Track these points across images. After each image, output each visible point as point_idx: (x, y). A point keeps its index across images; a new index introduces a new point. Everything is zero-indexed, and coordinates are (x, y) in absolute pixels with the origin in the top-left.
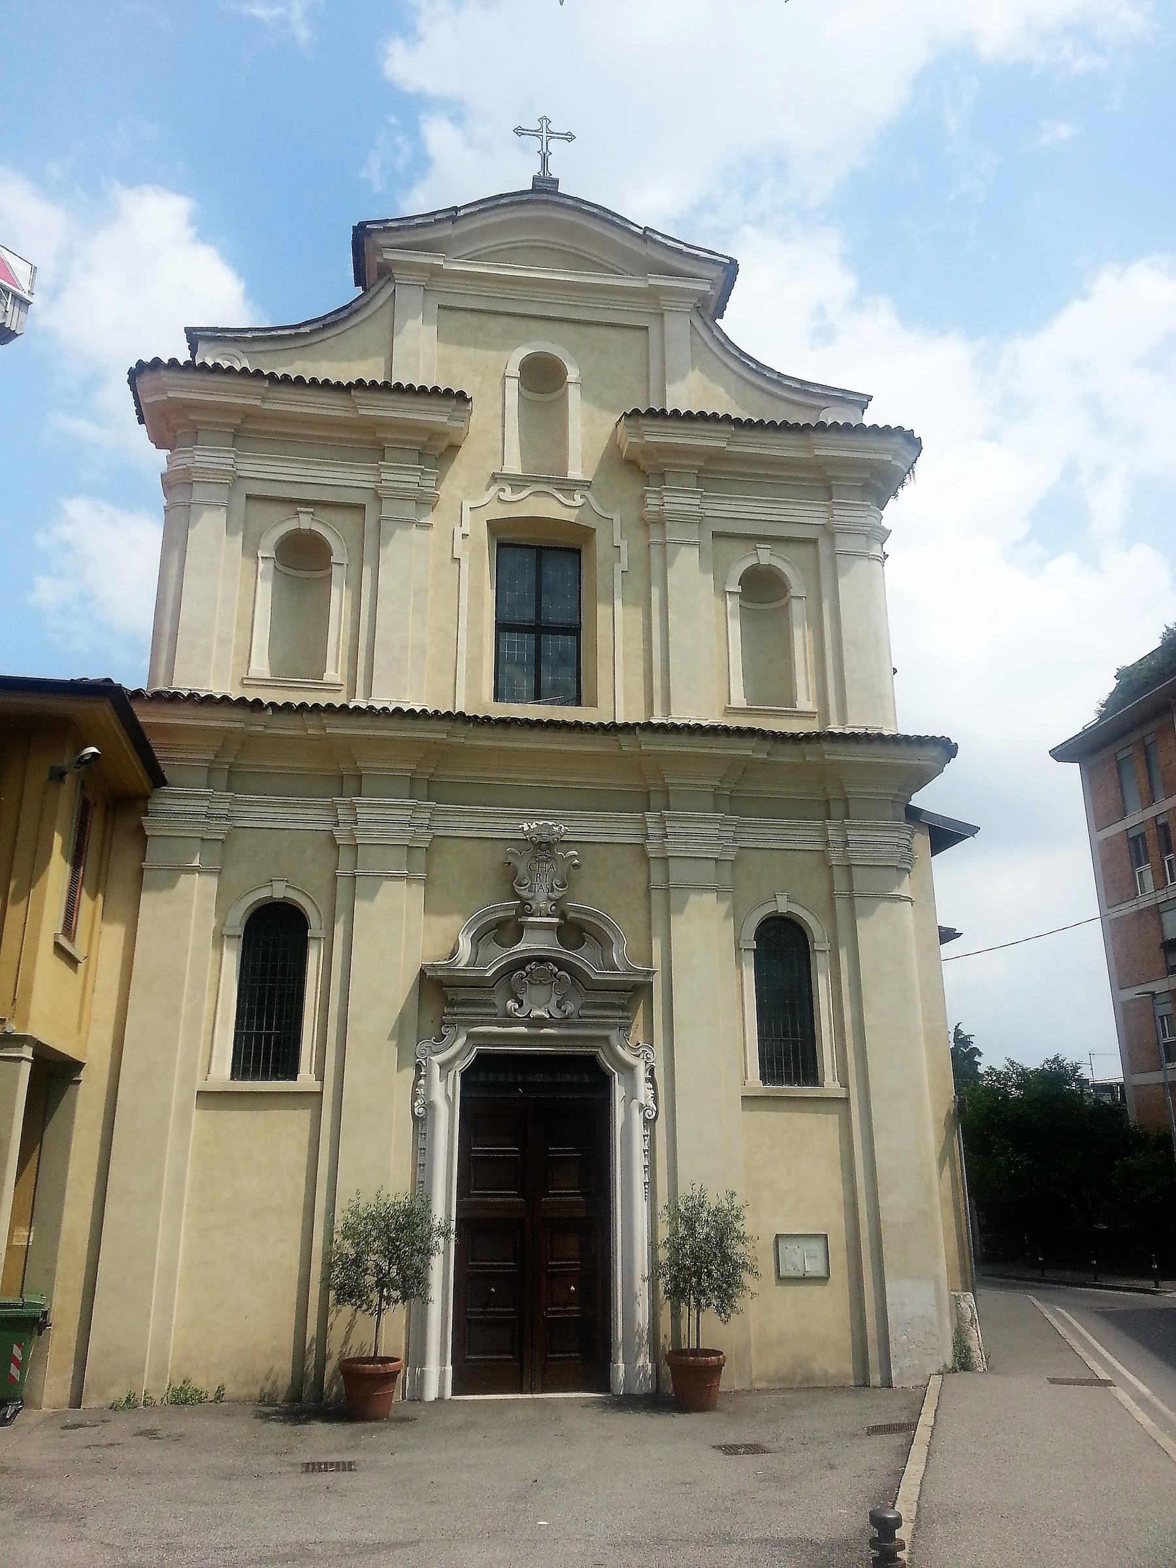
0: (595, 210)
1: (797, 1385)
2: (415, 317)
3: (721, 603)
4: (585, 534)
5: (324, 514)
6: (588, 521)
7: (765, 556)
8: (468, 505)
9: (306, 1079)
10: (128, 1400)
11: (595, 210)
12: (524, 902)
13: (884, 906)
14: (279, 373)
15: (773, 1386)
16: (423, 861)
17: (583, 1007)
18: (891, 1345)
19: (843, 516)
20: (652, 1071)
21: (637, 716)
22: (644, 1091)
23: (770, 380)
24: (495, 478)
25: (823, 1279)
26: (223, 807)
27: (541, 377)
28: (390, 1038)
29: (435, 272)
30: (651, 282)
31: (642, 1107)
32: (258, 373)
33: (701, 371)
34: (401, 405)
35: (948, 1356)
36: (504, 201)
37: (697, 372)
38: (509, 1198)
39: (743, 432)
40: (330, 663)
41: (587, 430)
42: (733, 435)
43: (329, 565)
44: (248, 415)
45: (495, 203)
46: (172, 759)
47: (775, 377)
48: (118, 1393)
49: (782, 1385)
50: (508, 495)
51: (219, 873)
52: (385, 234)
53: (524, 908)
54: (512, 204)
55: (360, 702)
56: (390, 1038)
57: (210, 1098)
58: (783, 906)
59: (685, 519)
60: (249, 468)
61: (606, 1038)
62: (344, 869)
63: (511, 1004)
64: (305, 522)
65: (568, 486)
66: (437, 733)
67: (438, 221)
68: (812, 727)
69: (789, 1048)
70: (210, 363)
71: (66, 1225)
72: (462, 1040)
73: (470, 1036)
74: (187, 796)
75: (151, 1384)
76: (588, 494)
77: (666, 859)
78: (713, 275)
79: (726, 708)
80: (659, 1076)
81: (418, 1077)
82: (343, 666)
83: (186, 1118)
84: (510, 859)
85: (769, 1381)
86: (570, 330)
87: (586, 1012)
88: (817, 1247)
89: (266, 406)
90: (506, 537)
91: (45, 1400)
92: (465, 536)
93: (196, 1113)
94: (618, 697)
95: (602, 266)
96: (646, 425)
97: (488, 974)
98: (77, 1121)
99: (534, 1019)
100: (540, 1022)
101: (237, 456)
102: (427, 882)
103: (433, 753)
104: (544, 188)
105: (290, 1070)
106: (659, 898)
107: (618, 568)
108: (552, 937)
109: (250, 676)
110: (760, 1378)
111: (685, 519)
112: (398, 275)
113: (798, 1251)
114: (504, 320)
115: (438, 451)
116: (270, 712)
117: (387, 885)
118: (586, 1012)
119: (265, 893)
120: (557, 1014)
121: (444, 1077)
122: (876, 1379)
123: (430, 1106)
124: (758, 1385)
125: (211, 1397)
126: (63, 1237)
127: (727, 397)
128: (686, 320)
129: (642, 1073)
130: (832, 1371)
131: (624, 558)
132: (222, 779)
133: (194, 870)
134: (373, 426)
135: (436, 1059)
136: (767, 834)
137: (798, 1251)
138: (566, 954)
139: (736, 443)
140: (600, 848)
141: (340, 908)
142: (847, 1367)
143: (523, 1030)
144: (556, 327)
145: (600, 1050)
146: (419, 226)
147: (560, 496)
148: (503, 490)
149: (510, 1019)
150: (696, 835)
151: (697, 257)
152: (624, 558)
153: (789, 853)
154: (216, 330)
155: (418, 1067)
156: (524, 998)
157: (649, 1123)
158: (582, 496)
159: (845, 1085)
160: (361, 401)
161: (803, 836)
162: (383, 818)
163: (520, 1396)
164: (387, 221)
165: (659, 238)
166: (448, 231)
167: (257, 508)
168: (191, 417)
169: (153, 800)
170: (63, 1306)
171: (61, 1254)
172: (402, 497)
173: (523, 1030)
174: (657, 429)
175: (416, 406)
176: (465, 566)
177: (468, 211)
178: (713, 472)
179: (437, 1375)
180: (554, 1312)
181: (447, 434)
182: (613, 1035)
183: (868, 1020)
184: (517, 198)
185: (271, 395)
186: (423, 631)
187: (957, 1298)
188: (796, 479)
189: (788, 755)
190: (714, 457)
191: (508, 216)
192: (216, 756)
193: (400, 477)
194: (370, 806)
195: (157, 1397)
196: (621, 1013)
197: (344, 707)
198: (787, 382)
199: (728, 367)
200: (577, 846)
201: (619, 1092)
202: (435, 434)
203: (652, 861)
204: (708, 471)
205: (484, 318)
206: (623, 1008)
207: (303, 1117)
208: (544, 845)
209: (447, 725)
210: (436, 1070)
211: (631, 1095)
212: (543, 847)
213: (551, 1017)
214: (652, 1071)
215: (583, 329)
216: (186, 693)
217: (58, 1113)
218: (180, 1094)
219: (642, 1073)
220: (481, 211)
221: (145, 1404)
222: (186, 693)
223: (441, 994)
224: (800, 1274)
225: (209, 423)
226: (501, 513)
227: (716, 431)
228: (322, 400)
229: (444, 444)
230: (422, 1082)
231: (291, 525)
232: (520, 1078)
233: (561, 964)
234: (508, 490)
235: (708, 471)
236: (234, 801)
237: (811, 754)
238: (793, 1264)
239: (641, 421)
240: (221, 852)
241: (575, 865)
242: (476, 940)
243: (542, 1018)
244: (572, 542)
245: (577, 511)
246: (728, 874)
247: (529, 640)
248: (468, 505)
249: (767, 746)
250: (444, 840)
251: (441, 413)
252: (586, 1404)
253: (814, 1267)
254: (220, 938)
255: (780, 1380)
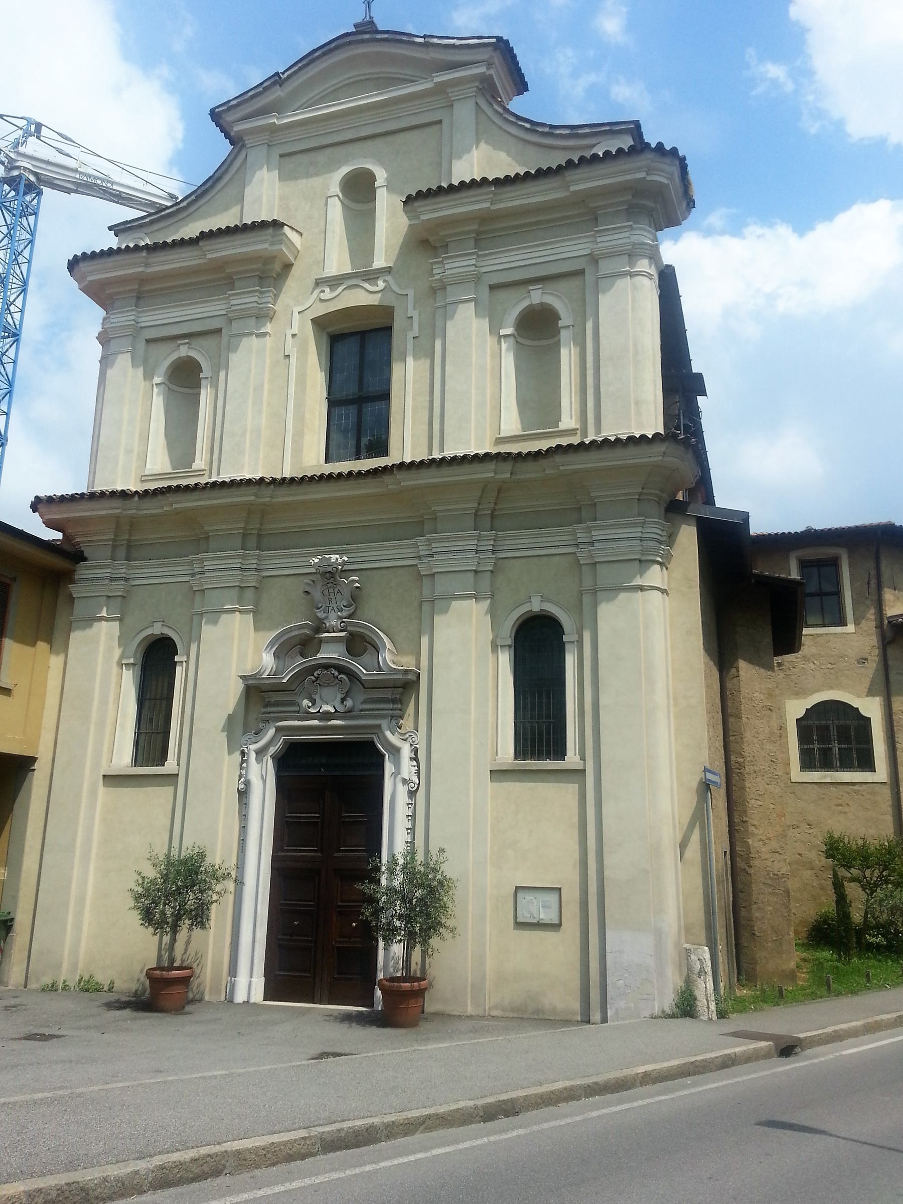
0: (386, 36)
1: (528, 1016)
2: (261, 168)
3: (496, 346)
4: (387, 312)
5: (197, 342)
6: (390, 301)
7: (537, 296)
8: (297, 310)
9: (572, 758)
10: (52, 986)
11: (386, 36)
12: (321, 621)
13: (623, 596)
14: (169, 240)
15: (507, 1014)
16: (254, 597)
17: (364, 702)
18: (609, 988)
19: (608, 241)
20: (416, 751)
21: (421, 455)
22: (407, 768)
23: (543, 134)
24: (318, 283)
25: (556, 927)
26: (122, 572)
27: (359, 189)
28: (223, 731)
29: (273, 129)
30: (436, 80)
31: (405, 782)
32: (136, 246)
33: (487, 143)
34: (235, 243)
35: (668, 1001)
36: (316, 54)
37: (483, 145)
38: (310, 853)
39: (504, 189)
40: (198, 455)
41: (390, 220)
42: (495, 194)
43: (556, 332)
44: (142, 280)
45: (309, 58)
46: (90, 541)
47: (547, 130)
48: (47, 980)
49: (515, 1015)
50: (328, 294)
51: (120, 620)
52: (230, 113)
53: (319, 627)
54: (324, 54)
55: (437, 455)
56: (223, 731)
57: (498, 774)
58: (536, 606)
59: (461, 281)
60: (147, 319)
61: (379, 727)
62: (587, 583)
63: (306, 702)
64: (184, 351)
65: (372, 276)
66: (504, 472)
67: (266, 89)
68: (575, 441)
69: (541, 729)
70: (131, 245)
71: (24, 868)
72: (271, 732)
73: (278, 730)
74: (95, 567)
75: (66, 975)
76: (388, 278)
77: (203, 591)
78: (485, 56)
79: (497, 439)
80: (422, 756)
81: (243, 762)
82: (206, 456)
83: (93, 793)
84: (307, 589)
85: (504, 1010)
86: (379, 143)
87: (364, 706)
88: (553, 898)
89: (149, 270)
90: (336, 328)
91: (12, 982)
92: (294, 336)
93: (101, 789)
94: (407, 443)
95: (398, 79)
96: (419, 207)
97: (285, 681)
98: (33, 797)
99: (323, 714)
100: (327, 716)
101: (479, 256)
102: (255, 613)
103: (258, 513)
104: (366, 30)
105: (560, 752)
106: (426, 606)
107: (410, 335)
108: (342, 648)
109: (146, 473)
110: (496, 1007)
111: (461, 281)
112: (248, 141)
113: (534, 901)
114: (328, 151)
115: (272, 273)
116: (136, 498)
117: (455, 604)
118: (364, 706)
119: (149, 632)
120: (340, 709)
121: (259, 759)
122: (596, 1016)
123: (247, 783)
124: (495, 1013)
125: (106, 988)
126: (23, 875)
127: (509, 160)
128: (471, 104)
129: (406, 752)
130: (560, 1006)
131: (416, 326)
132: (122, 552)
133: (102, 619)
134: (220, 266)
135: (253, 747)
136: (520, 542)
137: (534, 901)
138: (310, 661)
139: (501, 201)
140: (385, 572)
141: (194, 636)
142: (576, 1006)
143: (316, 722)
144: (369, 143)
145: (374, 736)
146: (252, 97)
147: (366, 285)
148: (323, 291)
149: (309, 716)
150: (456, 551)
151: (468, 46)
152: (416, 326)
153: (545, 558)
154: (126, 222)
155: (243, 754)
156: (317, 697)
157: (412, 794)
158: (384, 281)
159: (583, 758)
160: (208, 248)
161: (557, 540)
162: (221, 566)
163: (312, 1005)
164: (229, 101)
165: (435, 41)
166: (278, 93)
167: (153, 347)
168: (107, 292)
169: (78, 572)
170: (22, 919)
171: (22, 886)
172: (244, 315)
173: (316, 722)
174: (451, 203)
175: (259, 239)
176: (293, 360)
177: (289, 72)
178: (487, 232)
179: (251, 984)
180: (341, 942)
181: (274, 257)
182: (384, 723)
183: (603, 701)
184: (328, 48)
185: (151, 260)
186: (270, 416)
187: (688, 951)
188: (565, 218)
189: (529, 472)
190: (485, 218)
191: (324, 65)
192: (479, 504)
193: (244, 300)
194: (213, 559)
195: (71, 984)
196: (391, 706)
197: (582, 444)
198: (558, 132)
199: (508, 133)
200: (358, 573)
201: (389, 768)
202: (267, 260)
203: (584, 567)
204: (486, 232)
205: (312, 155)
206: (394, 701)
207: (572, 789)
208: (328, 575)
209: (253, 489)
210: (253, 756)
211: (397, 772)
212: (330, 576)
213: (336, 711)
214: (416, 751)
215: (390, 139)
216: (612, 439)
217: (22, 792)
218: (90, 777)
219: (406, 752)
220: (300, 69)
221: (63, 989)
222: (612, 439)
223: (259, 696)
224: (535, 921)
225: (119, 293)
226: (322, 310)
227: (480, 195)
228: (183, 255)
229: (277, 266)
230: (244, 765)
231: (174, 356)
232: (324, 761)
233: (341, 669)
234: (327, 290)
235: (486, 232)
236: (129, 567)
237: (547, 468)
238: (529, 912)
239: (416, 204)
240: (123, 605)
241: (357, 587)
242: (276, 656)
243: (328, 713)
244: (379, 322)
245: (380, 295)
246: (486, 582)
247: (352, 410)
248: (297, 310)
249: (508, 466)
250: (270, 579)
251: (262, 242)
252: (348, 1018)
253: (548, 915)
254: (495, 647)
255: (513, 1010)
